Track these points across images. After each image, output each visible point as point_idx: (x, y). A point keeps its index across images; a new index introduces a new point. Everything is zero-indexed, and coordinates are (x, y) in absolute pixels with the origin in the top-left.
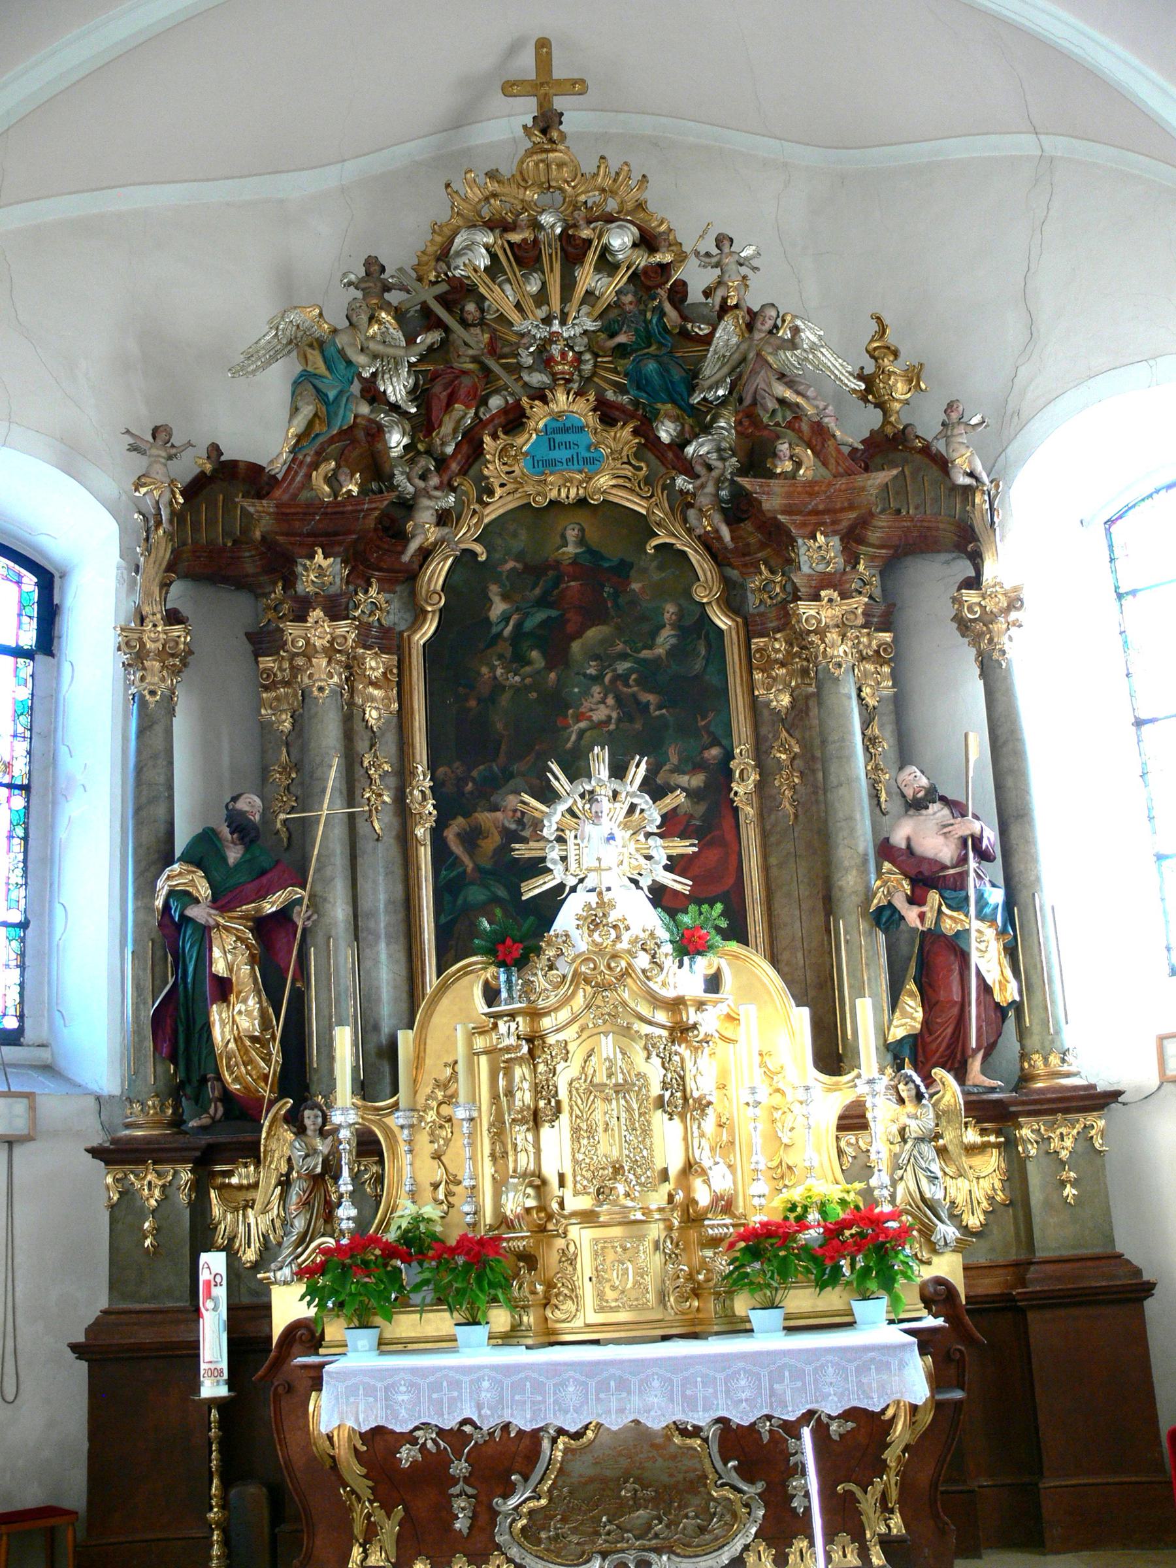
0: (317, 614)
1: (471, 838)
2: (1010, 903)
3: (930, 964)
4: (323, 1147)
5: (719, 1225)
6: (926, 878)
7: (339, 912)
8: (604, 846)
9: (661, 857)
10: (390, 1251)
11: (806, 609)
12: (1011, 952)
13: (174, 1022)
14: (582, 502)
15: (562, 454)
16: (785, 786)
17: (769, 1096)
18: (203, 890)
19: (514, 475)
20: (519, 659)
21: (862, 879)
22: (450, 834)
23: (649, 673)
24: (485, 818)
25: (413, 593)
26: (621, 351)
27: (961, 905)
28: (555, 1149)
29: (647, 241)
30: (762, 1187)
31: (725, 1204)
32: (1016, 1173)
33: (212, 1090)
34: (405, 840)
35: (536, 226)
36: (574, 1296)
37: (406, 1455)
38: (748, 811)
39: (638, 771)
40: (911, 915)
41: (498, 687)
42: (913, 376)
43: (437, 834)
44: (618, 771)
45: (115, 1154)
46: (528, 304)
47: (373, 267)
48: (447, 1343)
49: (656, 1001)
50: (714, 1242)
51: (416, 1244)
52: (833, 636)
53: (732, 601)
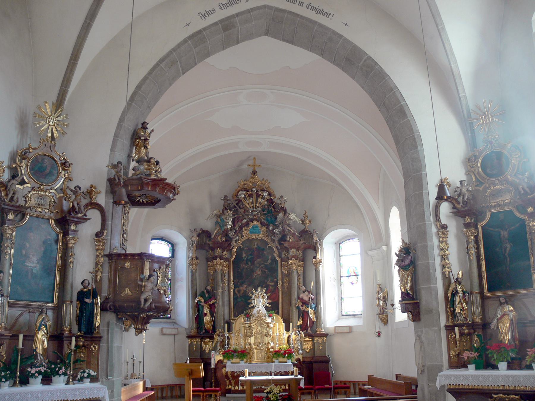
0: (218, 259)
1: (239, 291)
2: (316, 307)
3: (304, 315)
4: (222, 338)
5: (272, 350)
6: (305, 303)
7: (221, 303)
8: (260, 302)
9: (267, 302)
10: (232, 351)
11: (290, 261)
12: (315, 313)
13: (199, 319)
14: (257, 239)
15: (255, 231)
16: (286, 285)
17: (279, 333)
18: (203, 301)
19: (246, 233)
20: (247, 263)
21: (296, 302)
22: (236, 290)
23: (266, 267)
24: (241, 288)
25: (231, 252)
26: (265, 214)
27: (308, 307)
28: (252, 340)
29: (270, 194)
30: (277, 345)
31: (272, 348)
32: (313, 345)
33: (203, 328)
34: (229, 291)
35: (252, 191)
36: (254, 358)
37: (236, 374)
38: (280, 289)
39: (264, 290)
40: (301, 308)
41: (244, 268)
42: (310, 221)
43: (234, 291)
44: (262, 291)
45: (189, 337)
46: (250, 204)
47: (226, 197)
48: (239, 362)
49: (265, 323)
50: (271, 352)
51: (235, 351)
52: (294, 265)
53: (280, 256)
